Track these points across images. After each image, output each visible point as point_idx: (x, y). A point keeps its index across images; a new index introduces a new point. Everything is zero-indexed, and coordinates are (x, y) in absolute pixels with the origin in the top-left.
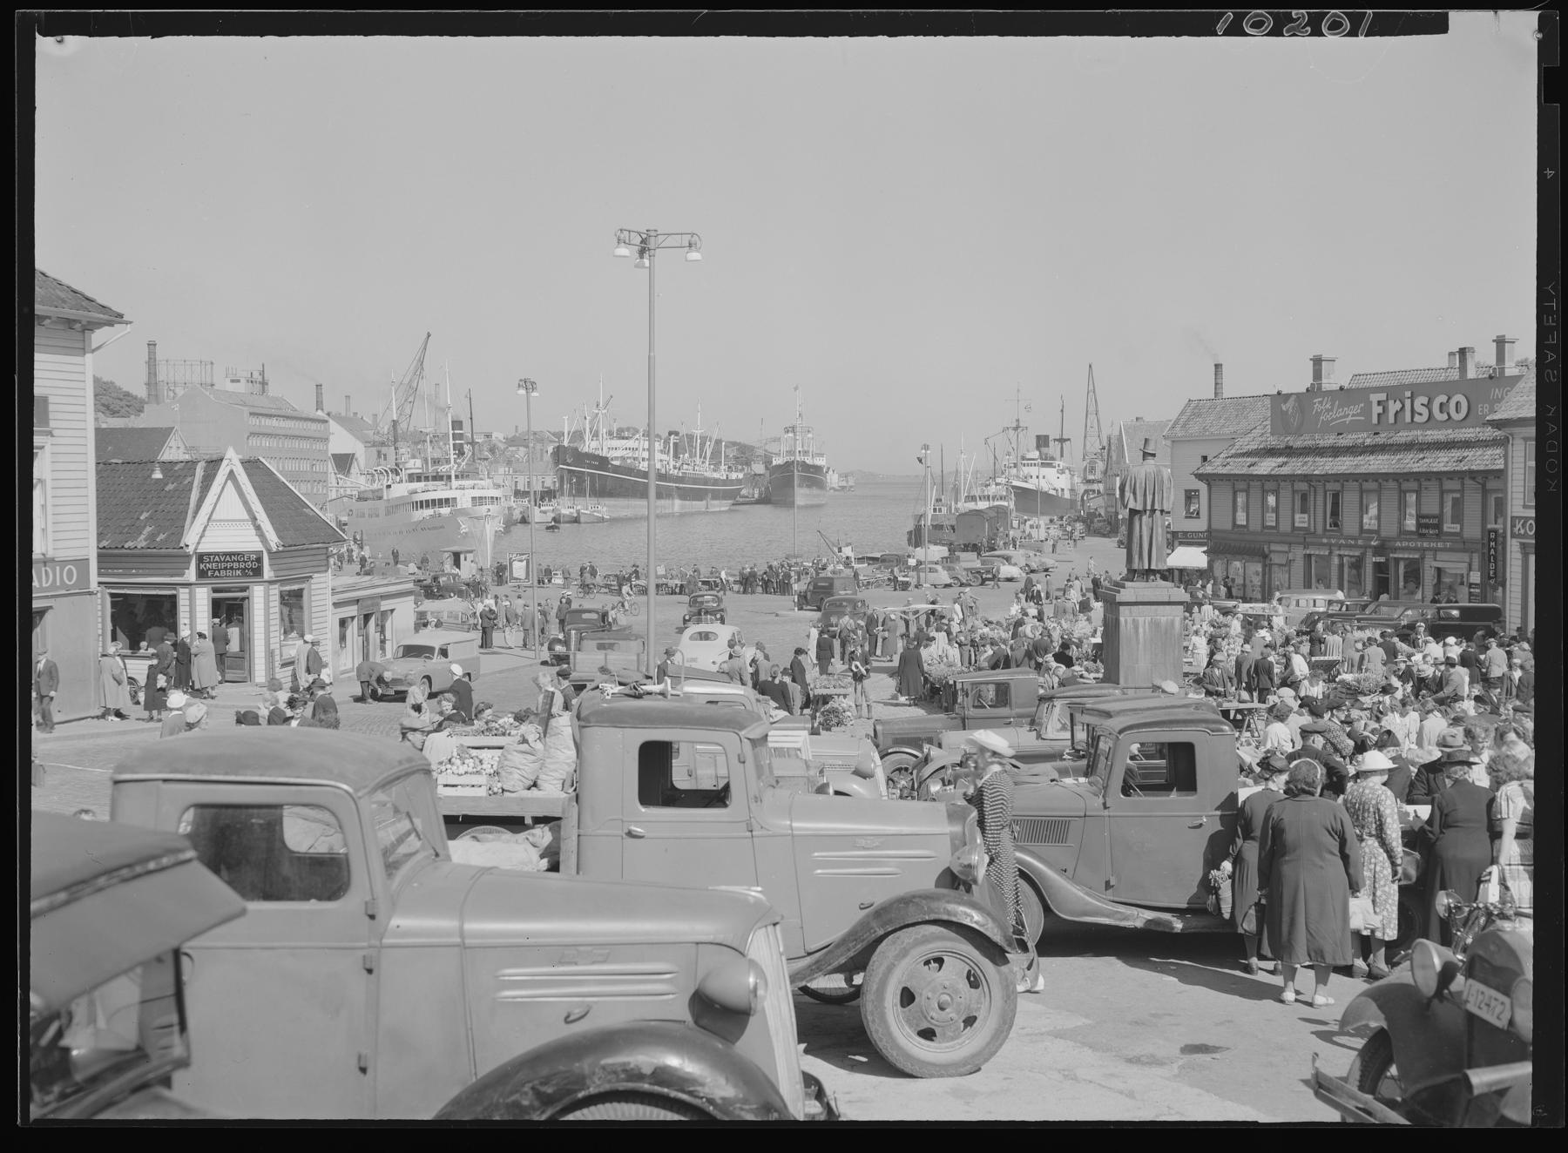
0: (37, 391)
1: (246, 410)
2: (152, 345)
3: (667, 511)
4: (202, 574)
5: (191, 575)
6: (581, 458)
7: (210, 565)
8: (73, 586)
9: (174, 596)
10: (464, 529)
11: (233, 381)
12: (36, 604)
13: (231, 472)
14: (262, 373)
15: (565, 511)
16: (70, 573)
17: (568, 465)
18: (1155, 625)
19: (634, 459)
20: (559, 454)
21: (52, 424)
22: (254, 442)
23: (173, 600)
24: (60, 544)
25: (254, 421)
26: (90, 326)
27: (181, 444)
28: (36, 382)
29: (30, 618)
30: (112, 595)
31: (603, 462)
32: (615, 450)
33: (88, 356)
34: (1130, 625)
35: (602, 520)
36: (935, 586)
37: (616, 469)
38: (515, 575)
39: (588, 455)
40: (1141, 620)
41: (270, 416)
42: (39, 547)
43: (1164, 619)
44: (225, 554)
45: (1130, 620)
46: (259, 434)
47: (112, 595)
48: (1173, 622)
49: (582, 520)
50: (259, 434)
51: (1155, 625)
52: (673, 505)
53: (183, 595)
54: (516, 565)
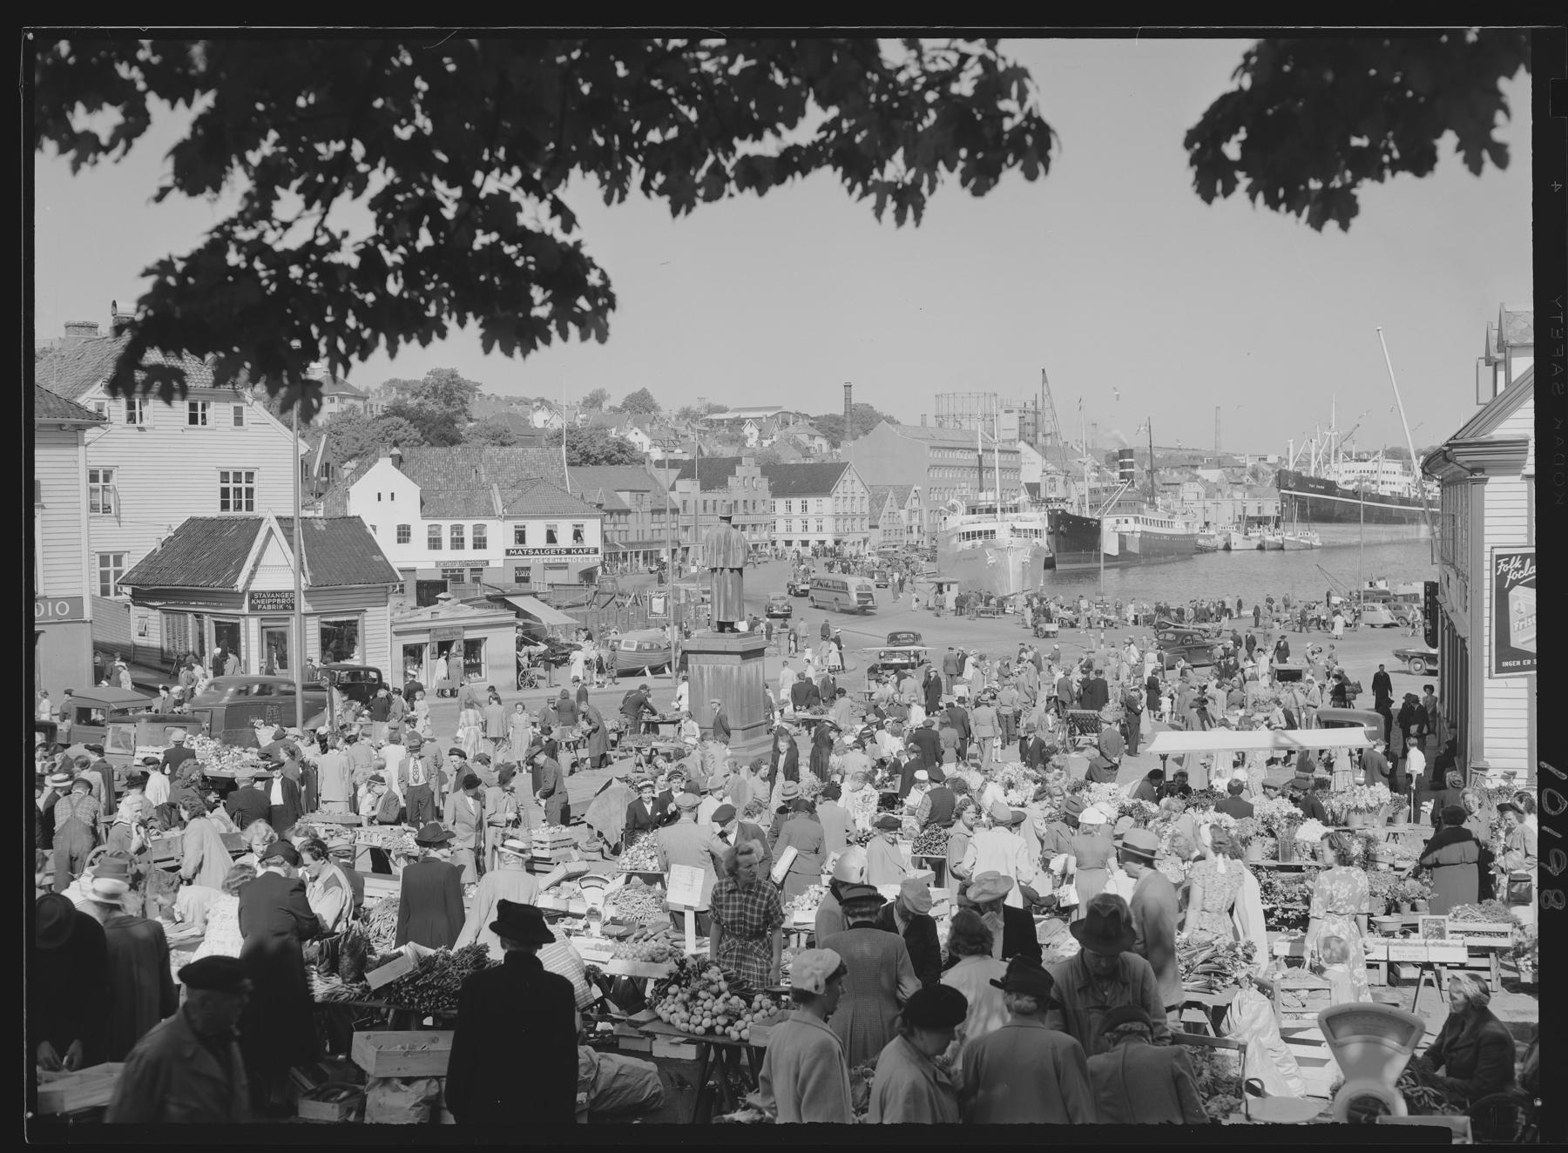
0: (36, 477)
1: (926, 444)
2: (848, 386)
3: (1410, 537)
4: (253, 608)
5: (246, 609)
6: (1302, 482)
7: (259, 601)
8: (66, 617)
9: (353, 624)
10: (991, 560)
11: (1006, 412)
12: (37, 628)
13: (270, 529)
14: (1035, 403)
15: (1270, 538)
16: (62, 608)
17: (1290, 489)
18: (717, 672)
19: (1373, 482)
20: (1282, 479)
21: (43, 500)
22: (935, 474)
23: (237, 625)
24: (48, 587)
25: (938, 455)
26: (80, 428)
27: (855, 478)
28: (36, 471)
29: (33, 637)
30: (216, 622)
31: (1330, 487)
32: (1343, 474)
33: (81, 448)
34: (697, 672)
35: (1311, 547)
36: (1373, 626)
37: (1345, 494)
38: (654, 610)
39: (1311, 480)
40: (705, 667)
41: (953, 449)
42: (41, 588)
43: (724, 667)
44: (272, 592)
45: (696, 667)
46: (940, 467)
47: (216, 622)
48: (732, 669)
49: (1286, 547)
50: (940, 467)
51: (717, 672)
52: (1418, 531)
53: (242, 621)
54: (655, 601)
